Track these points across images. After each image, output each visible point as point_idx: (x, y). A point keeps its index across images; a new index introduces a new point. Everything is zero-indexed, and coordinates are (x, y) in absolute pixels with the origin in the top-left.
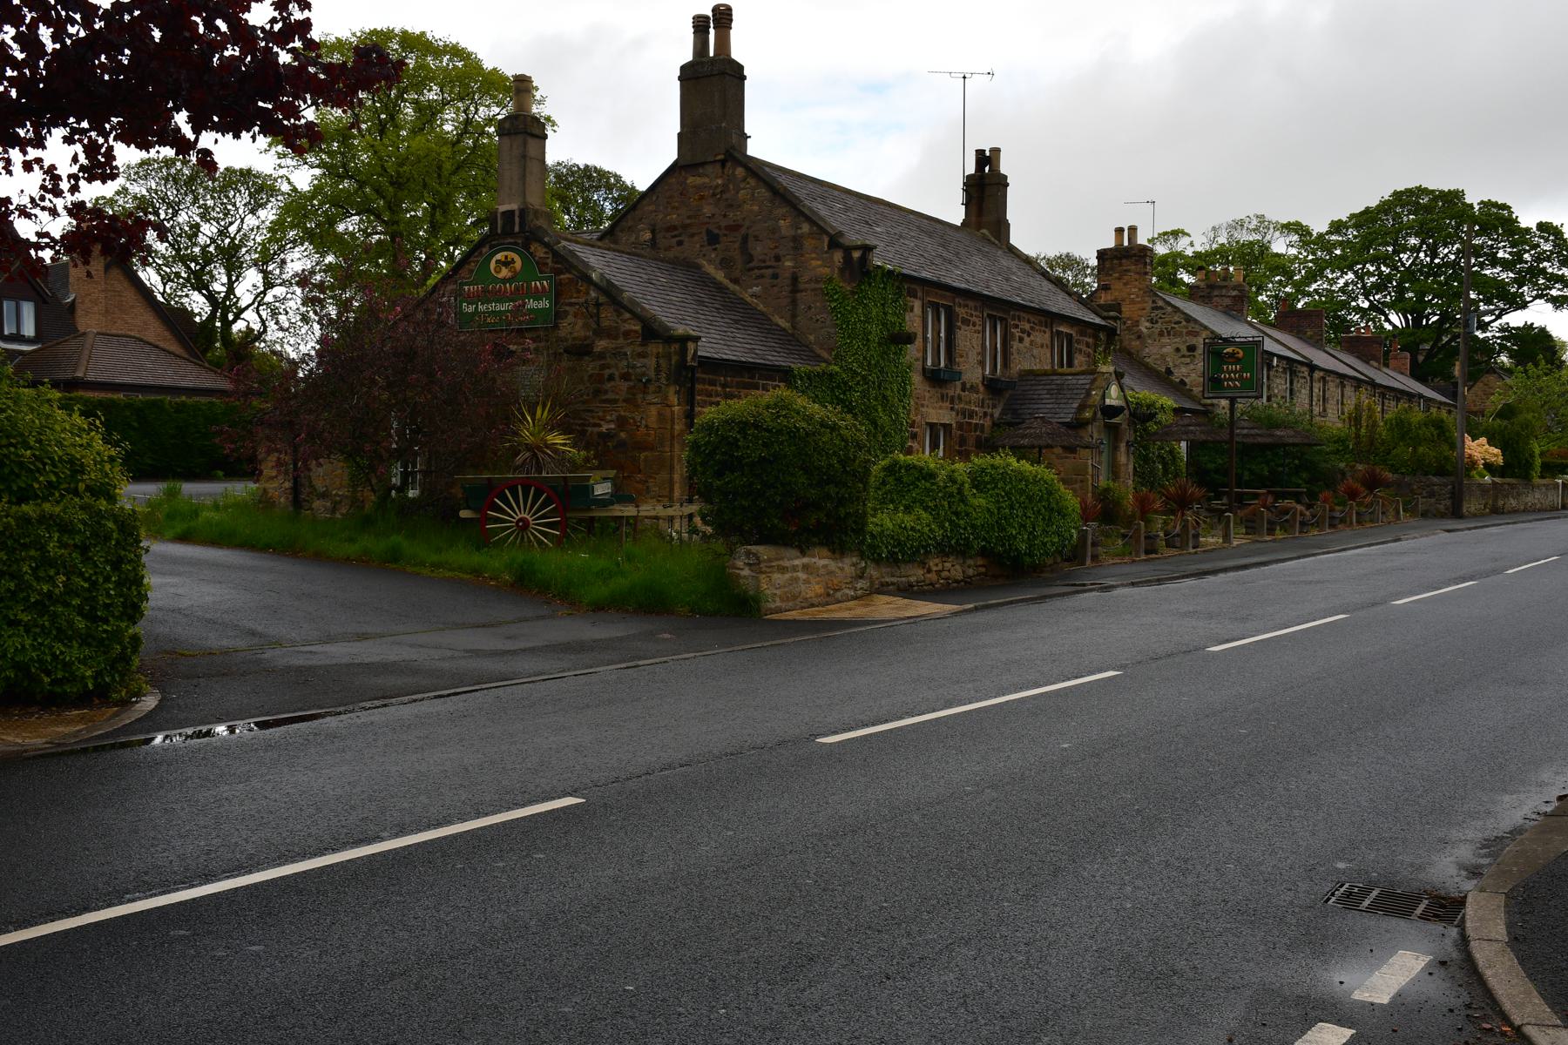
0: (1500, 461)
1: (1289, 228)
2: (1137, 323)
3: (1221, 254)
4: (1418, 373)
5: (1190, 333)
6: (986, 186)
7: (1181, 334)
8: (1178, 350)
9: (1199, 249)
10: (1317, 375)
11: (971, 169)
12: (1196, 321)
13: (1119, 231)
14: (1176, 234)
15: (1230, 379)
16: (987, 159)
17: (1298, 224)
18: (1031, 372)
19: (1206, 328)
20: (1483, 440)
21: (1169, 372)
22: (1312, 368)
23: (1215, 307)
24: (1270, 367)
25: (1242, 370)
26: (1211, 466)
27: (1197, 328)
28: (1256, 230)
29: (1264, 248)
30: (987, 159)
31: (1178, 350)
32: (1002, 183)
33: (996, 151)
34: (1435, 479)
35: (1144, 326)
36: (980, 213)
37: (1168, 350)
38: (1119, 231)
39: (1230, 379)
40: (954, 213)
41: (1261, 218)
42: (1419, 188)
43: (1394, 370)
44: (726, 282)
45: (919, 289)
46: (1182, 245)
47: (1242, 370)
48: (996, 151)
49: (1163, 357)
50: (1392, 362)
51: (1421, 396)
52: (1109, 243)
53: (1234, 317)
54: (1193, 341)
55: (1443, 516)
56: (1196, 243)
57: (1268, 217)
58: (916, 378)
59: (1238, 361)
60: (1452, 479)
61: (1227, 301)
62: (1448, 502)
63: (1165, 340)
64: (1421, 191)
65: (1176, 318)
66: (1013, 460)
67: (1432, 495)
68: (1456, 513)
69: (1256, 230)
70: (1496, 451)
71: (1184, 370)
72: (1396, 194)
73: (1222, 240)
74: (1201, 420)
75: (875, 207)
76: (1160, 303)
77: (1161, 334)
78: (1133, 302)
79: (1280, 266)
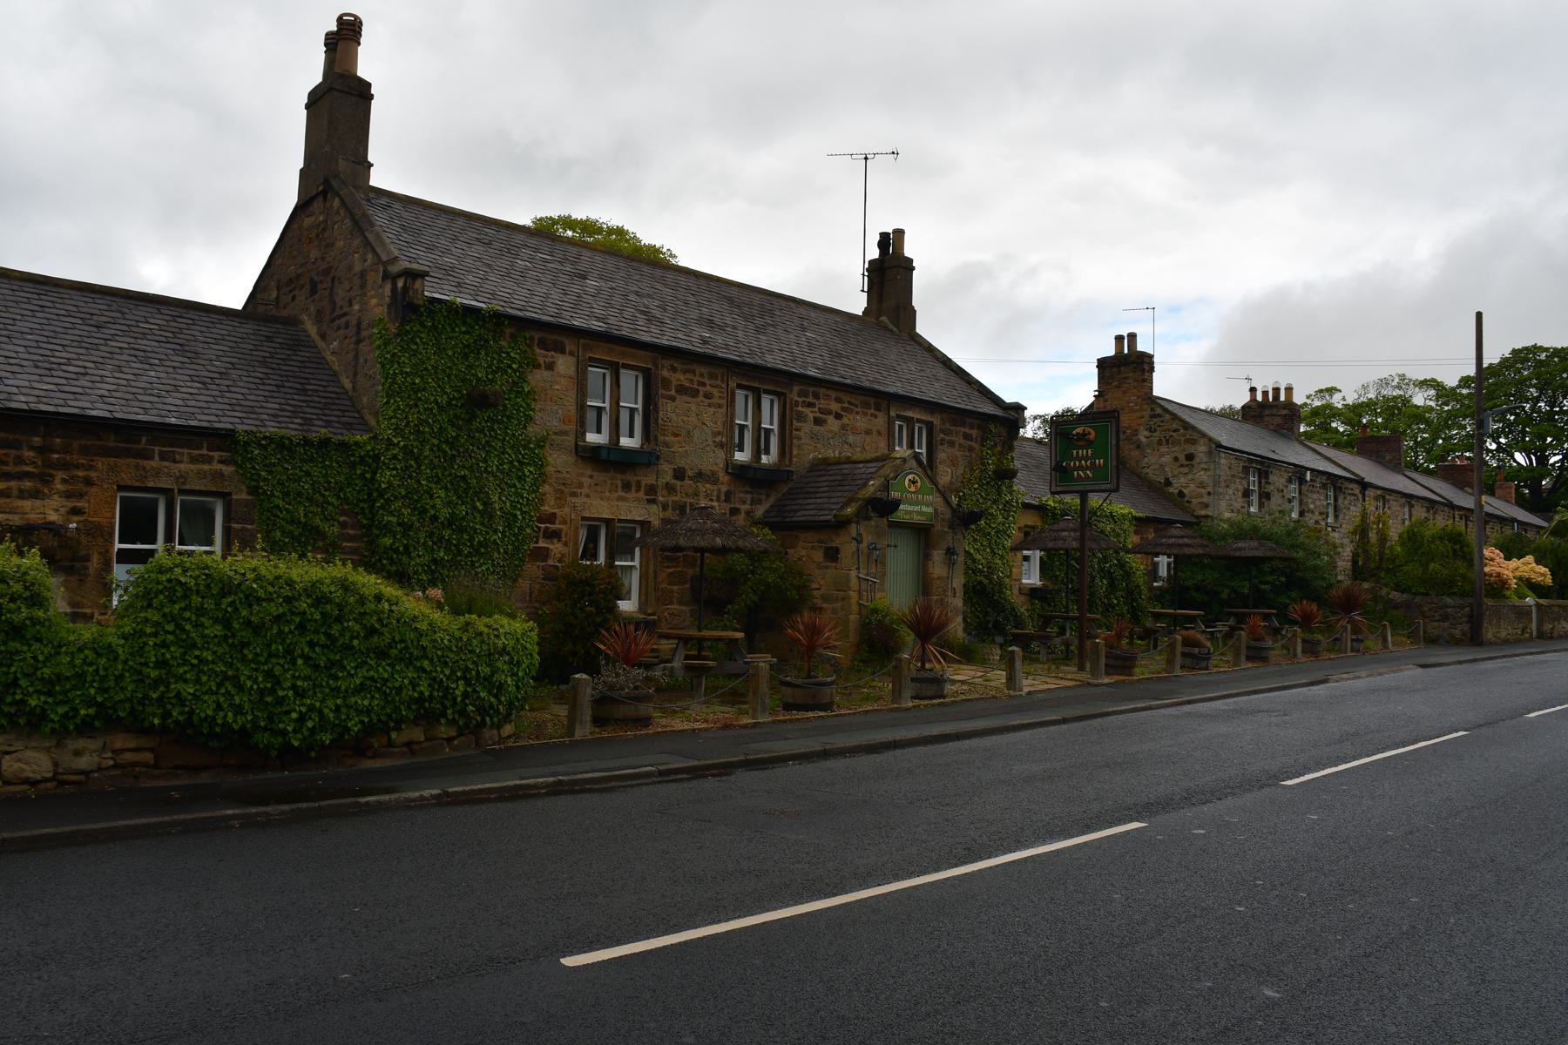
0: (1549, 580)
1: (1424, 384)
2: (1136, 433)
3: (1369, 406)
4: (1521, 502)
5: (1188, 441)
6: (890, 270)
7: (1178, 443)
8: (1176, 459)
9: (1350, 401)
10: (1370, 492)
11: (874, 253)
12: (1194, 428)
13: (1119, 339)
14: (1331, 391)
15: (1081, 468)
16: (891, 243)
17: (1433, 380)
18: (826, 462)
19: (1204, 435)
20: (1530, 558)
21: (1168, 483)
22: (1364, 486)
23: (1267, 427)
24: (1302, 481)
25: (1094, 457)
26: (1189, 583)
27: (1195, 436)
28: (1399, 387)
29: (1406, 401)
30: (891, 243)
31: (1176, 459)
32: (908, 266)
33: (899, 233)
34: (1449, 600)
35: (1143, 435)
36: (880, 301)
37: (1167, 459)
38: (1119, 339)
39: (1081, 468)
40: (856, 303)
41: (1402, 377)
42: (1535, 346)
43: (1500, 498)
44: (317, 338)
45: (872, 401)
46: (1337, 401)
47: (1094, 457)
48: (899, 233)
49: (1162, 467)
50: (1498, 492)
51: (1514, 520)
52: (1110, 351)
53: (1282, 435)
54: (1191, 449)
55: (1457, 642)
56: (1349, 395)
57: (1408, 375)
58: (559, 461)
59: (1090, 443)
60: (1471, 600)
61: (1278, 420)
62: (1466, 627)
63: (1164, 449)
64: (1536, 349)
65: (1174, 426)
66: (295, 574)
67: (1445, 618)
68: (1474, 639)
69: (1399, 387)
70: (1544, 570)
71: (1182, 480)
72: (1514, 352)
73: (1372, 396)
74: (1189, 532)
75: (802, 310)
76: (1159, 411)
77: (1160, 443)
78: (1132, 411)
79: (1419, 415)
